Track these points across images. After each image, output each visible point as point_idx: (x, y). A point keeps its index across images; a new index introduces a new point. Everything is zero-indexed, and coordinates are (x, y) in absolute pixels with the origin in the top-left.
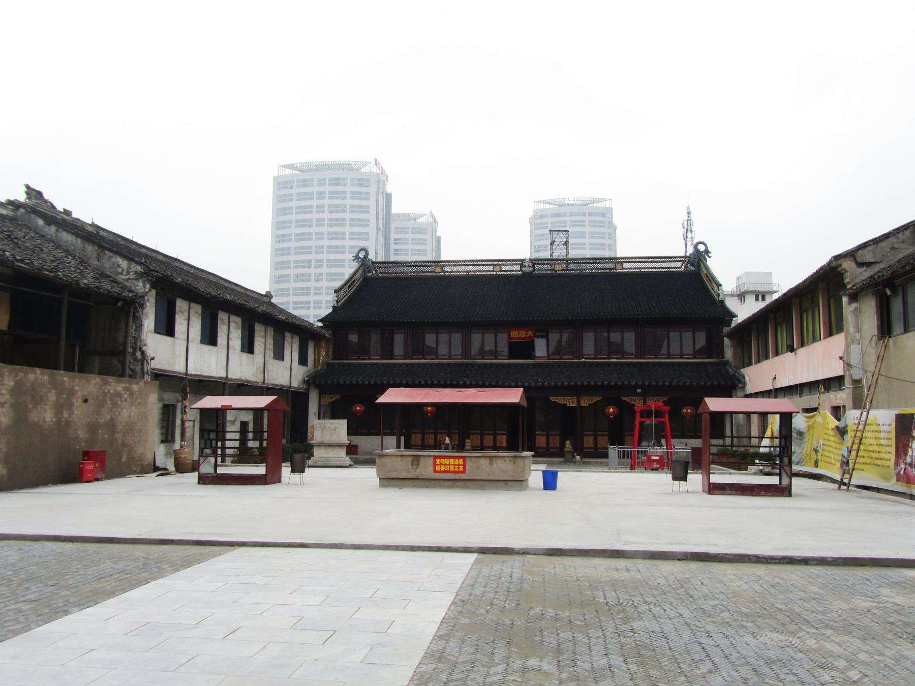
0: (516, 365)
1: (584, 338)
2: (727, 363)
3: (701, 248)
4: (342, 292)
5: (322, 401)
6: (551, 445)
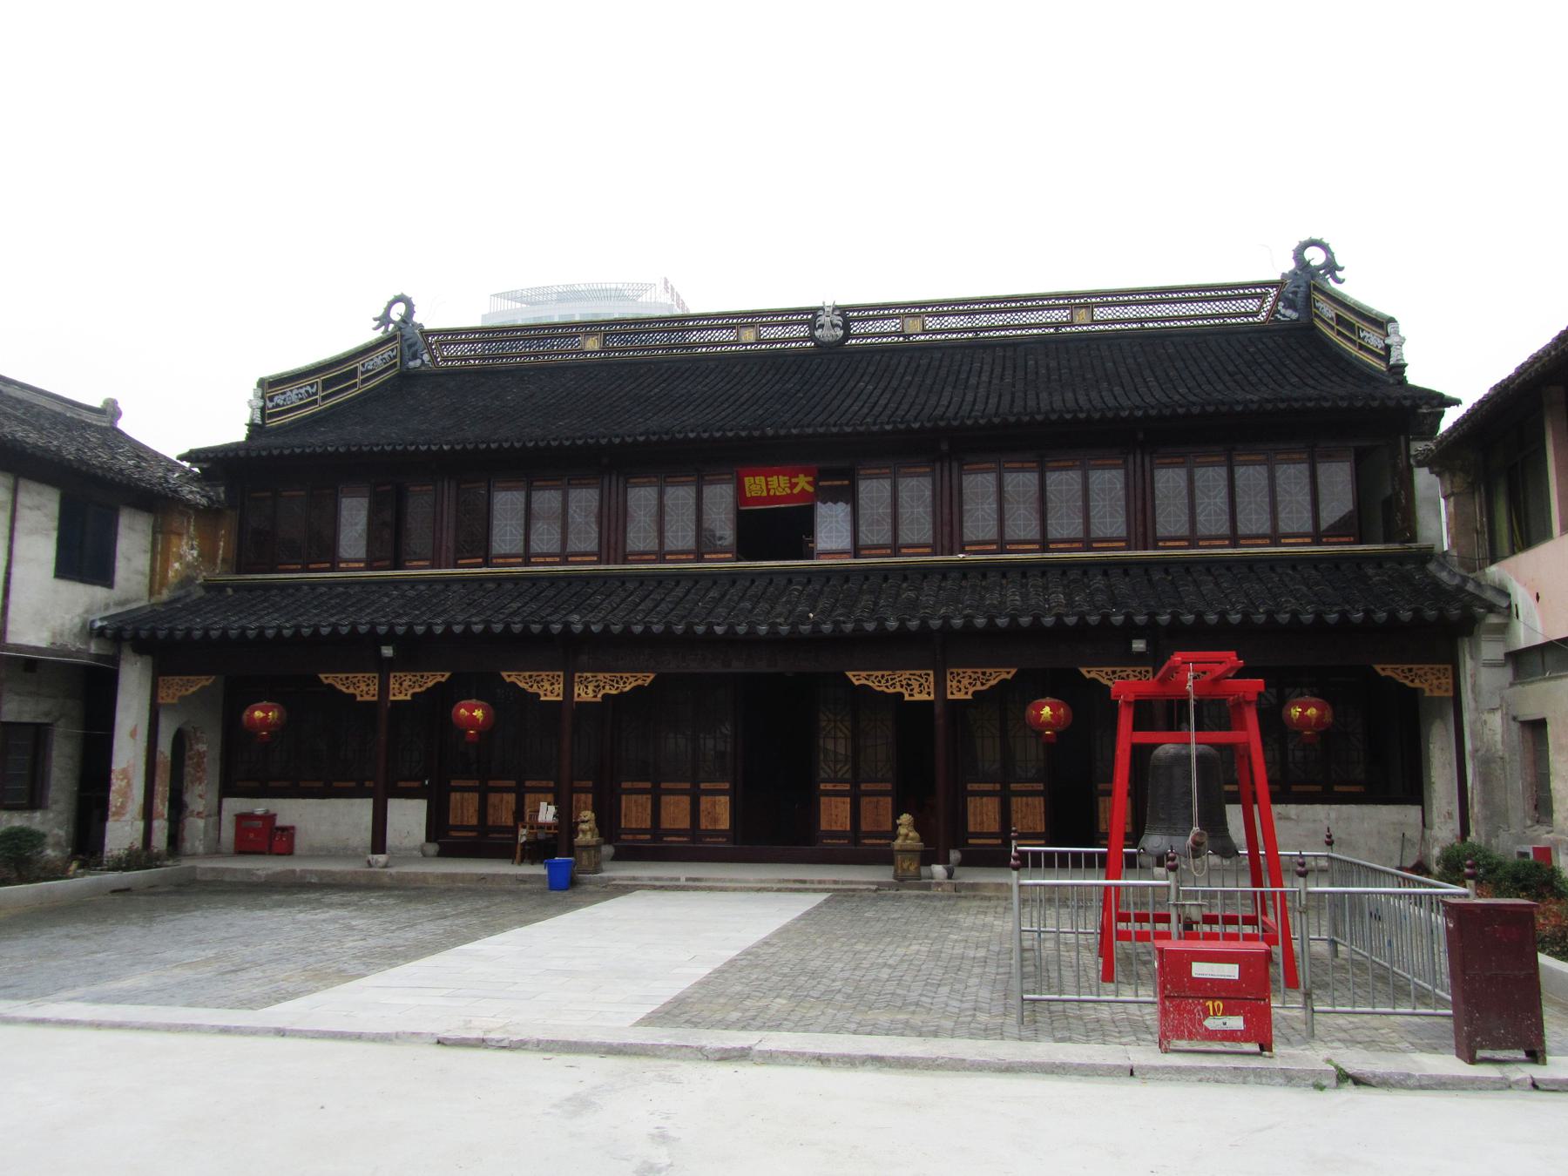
1: (967, 491)
2: (1427, 555)
3: (1315, 257)
4: (293, 395)
5: (162, 693)
6: (865, 826)
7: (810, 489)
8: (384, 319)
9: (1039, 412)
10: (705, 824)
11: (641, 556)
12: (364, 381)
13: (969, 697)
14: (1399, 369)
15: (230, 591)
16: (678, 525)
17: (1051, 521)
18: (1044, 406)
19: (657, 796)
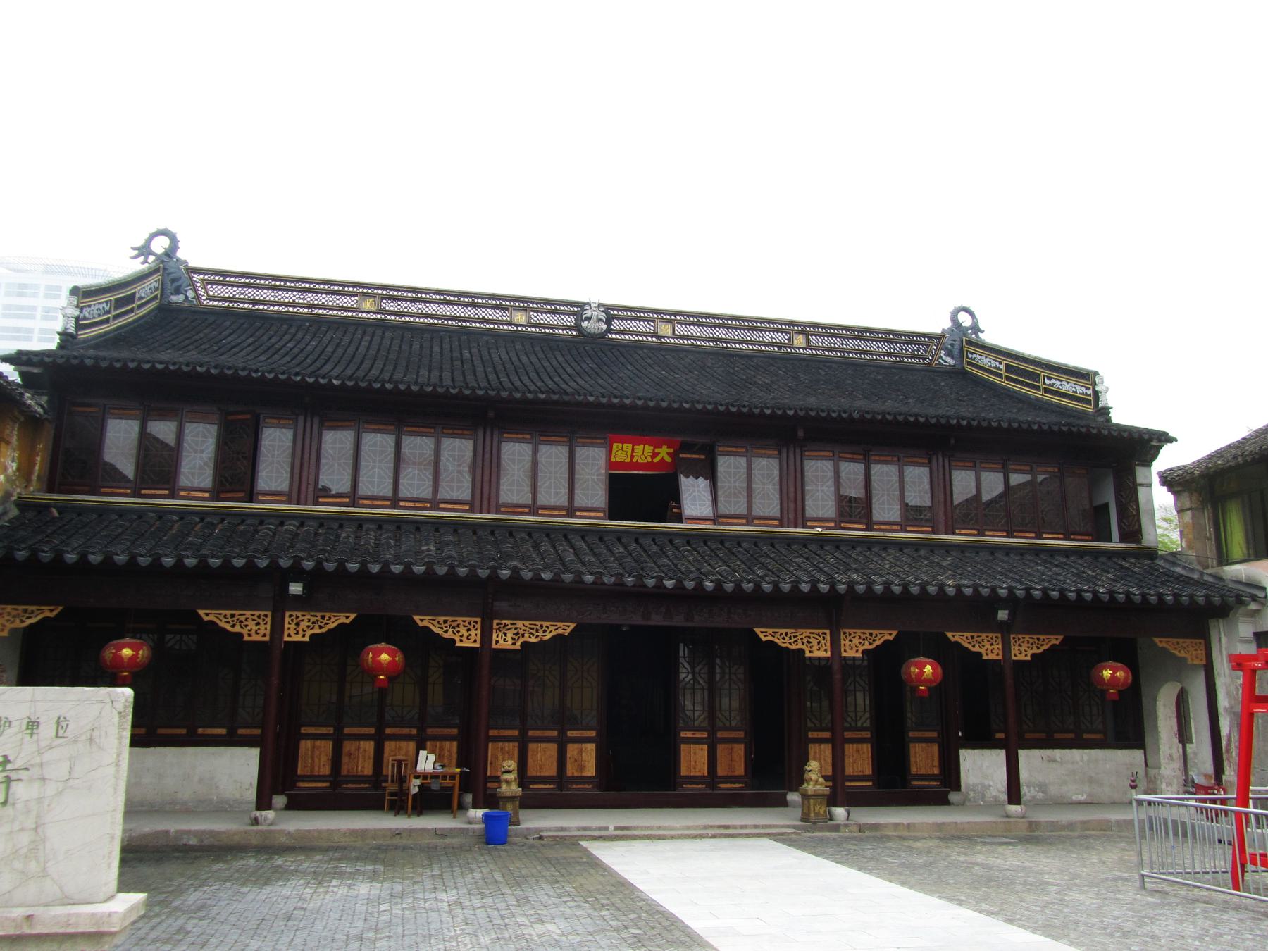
0: (637, 536)
3: (965, 319)
7: (668, 459)
8: (144, 251)
9: (428, 385)
10: (571, 771)
11: (514, 507)
12: (140, 307)
13: (1029, 658)
14: (1106, 411)
15: (55, 512)
16: (556, 482)
17: (578, 492)
18: (447, 381)
19: (379, 740)
